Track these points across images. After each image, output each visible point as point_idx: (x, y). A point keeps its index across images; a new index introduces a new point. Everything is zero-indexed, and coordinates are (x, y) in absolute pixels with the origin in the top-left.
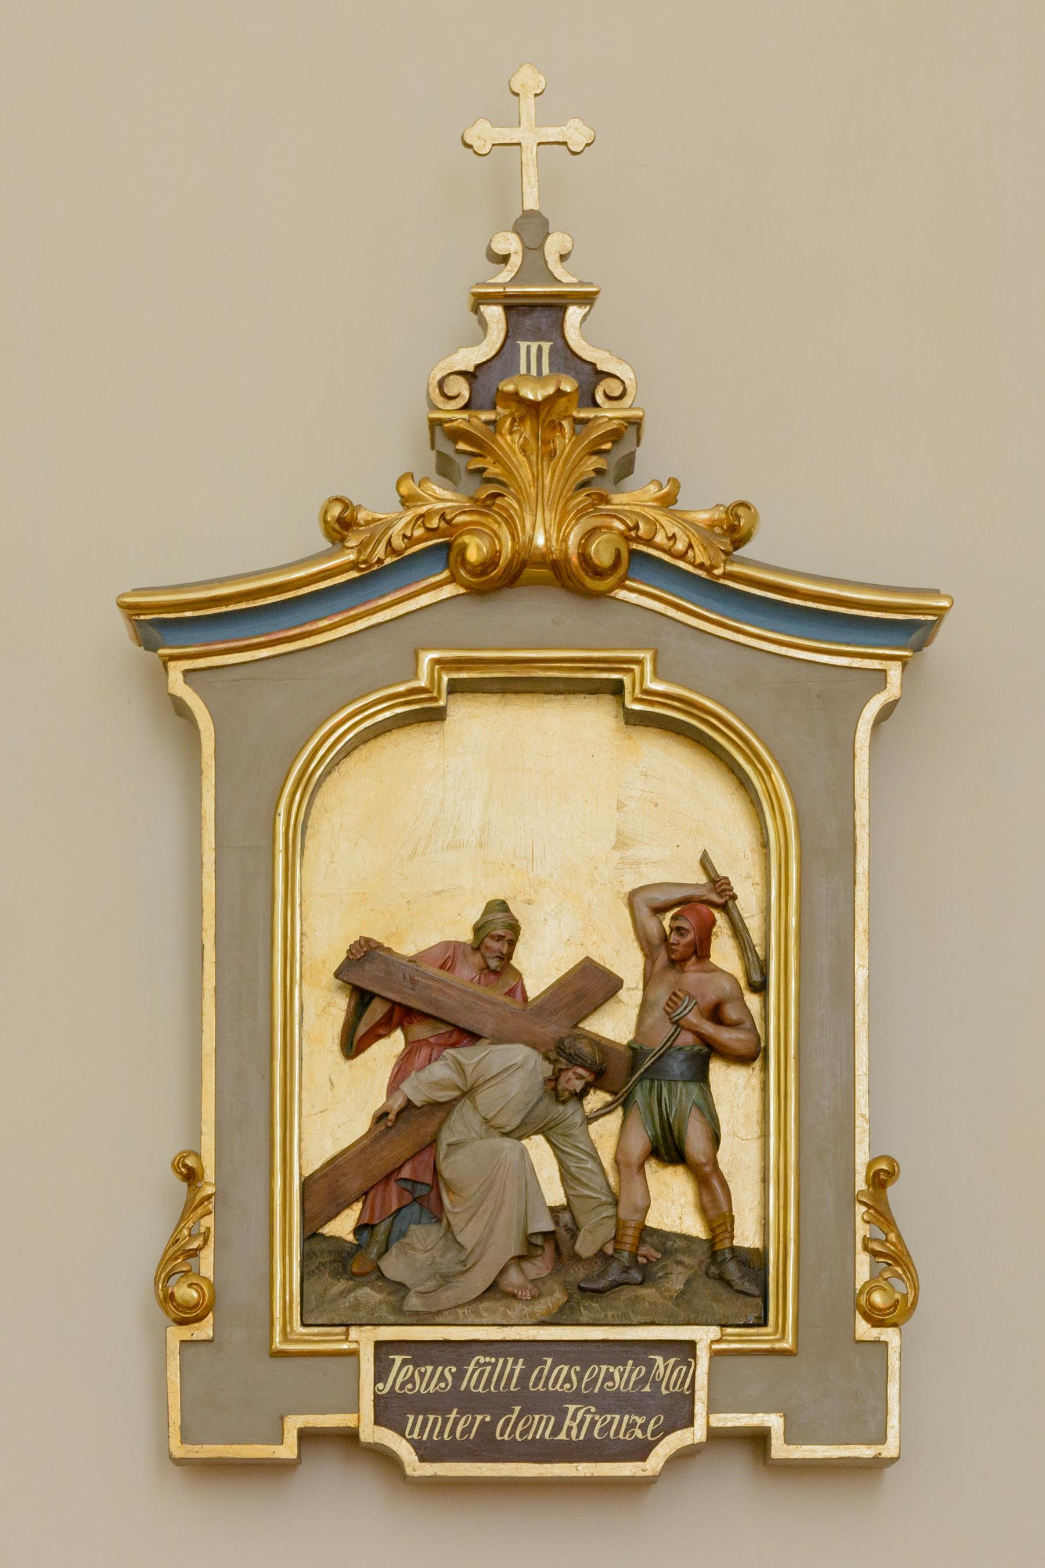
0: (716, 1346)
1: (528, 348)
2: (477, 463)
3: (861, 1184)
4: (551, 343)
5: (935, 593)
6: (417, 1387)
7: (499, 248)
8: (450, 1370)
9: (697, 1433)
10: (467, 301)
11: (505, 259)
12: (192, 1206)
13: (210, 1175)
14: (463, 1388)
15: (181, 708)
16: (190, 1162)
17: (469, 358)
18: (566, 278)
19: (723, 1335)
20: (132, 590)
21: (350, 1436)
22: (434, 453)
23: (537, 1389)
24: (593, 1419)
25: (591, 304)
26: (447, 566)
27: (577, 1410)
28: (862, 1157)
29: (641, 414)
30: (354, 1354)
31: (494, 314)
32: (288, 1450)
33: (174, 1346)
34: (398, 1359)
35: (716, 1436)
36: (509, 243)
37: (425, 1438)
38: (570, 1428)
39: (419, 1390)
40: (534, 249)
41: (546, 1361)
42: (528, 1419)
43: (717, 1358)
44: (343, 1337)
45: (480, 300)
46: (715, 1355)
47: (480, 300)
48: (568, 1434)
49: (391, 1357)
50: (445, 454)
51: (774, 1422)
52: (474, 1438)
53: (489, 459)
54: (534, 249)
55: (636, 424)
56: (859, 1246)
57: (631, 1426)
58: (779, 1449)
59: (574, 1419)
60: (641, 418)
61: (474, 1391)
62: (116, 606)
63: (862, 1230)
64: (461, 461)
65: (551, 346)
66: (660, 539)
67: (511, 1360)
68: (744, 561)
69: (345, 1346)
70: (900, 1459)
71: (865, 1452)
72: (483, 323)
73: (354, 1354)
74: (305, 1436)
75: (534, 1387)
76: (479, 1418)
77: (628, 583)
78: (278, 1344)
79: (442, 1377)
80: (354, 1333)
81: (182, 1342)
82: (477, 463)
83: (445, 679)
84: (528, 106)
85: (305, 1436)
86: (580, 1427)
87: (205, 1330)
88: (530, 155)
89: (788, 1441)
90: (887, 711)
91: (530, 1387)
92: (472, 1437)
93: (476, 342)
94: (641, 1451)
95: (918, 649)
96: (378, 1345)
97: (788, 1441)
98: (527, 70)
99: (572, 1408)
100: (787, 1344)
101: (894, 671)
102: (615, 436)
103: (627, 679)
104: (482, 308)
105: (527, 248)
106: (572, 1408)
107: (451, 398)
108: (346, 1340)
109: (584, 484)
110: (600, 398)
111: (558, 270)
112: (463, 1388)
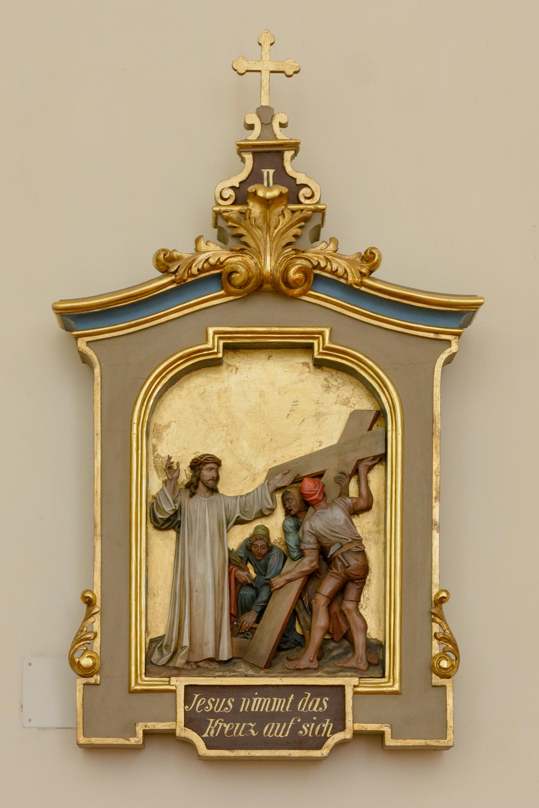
1: (268, 173)
5: (474, 297)
7: (249, 122)
9: (347, 735)
10: (235, 148)
11: (251, 127)
13: (98, 603)
14: (241, 710)
15: (85, 359)
18: (281, 136)
19: (360, 684)
20: (60, 301)
21: (170, 734)
24: (223, 726)
25: (296, 154)
26: (222, 288)
30: (174, 691)
31: (249, 158)
32: (137, 740)
35: (357, 734)
36: (253, 119)
40: (267, 124)
41: (307, 694)
44: (168, 683)
46: (355, 693)
47: (242, 149)
48: (209, 734)
49: (274, 698)
50: (221, 227)
54: (267, 124)
55: (323, 211)
56: (99, 635)
57: (247, 728)
58: (389, 742)
59: (213, 725)
60: (324, 209)
61: (217, 712)
62: (52, 309)
64: (229, 231)
68: (374, 279)
70: (454, 746)
71: (442, 743)
72: (243, 160)
73: (174, 691)
74: (147, 734)
77: (311, 292)
79: (226, 705)
80: (173, 680)
83: (221, 342)
85: (147, 734)
86: (216, 729)
87: (97, 678)
88: (266, 75)
90: (449, 360)
91: (197, 710)
95: (465, 326)
99: (212, 720)
100: (396, 687)
103: (316, 342)
105: (264, 124)
106: (212, 720)
107: (225, 200)
108: (169, 684)
109: (289, 244)
110: (302, 199)
112: (241, 710)
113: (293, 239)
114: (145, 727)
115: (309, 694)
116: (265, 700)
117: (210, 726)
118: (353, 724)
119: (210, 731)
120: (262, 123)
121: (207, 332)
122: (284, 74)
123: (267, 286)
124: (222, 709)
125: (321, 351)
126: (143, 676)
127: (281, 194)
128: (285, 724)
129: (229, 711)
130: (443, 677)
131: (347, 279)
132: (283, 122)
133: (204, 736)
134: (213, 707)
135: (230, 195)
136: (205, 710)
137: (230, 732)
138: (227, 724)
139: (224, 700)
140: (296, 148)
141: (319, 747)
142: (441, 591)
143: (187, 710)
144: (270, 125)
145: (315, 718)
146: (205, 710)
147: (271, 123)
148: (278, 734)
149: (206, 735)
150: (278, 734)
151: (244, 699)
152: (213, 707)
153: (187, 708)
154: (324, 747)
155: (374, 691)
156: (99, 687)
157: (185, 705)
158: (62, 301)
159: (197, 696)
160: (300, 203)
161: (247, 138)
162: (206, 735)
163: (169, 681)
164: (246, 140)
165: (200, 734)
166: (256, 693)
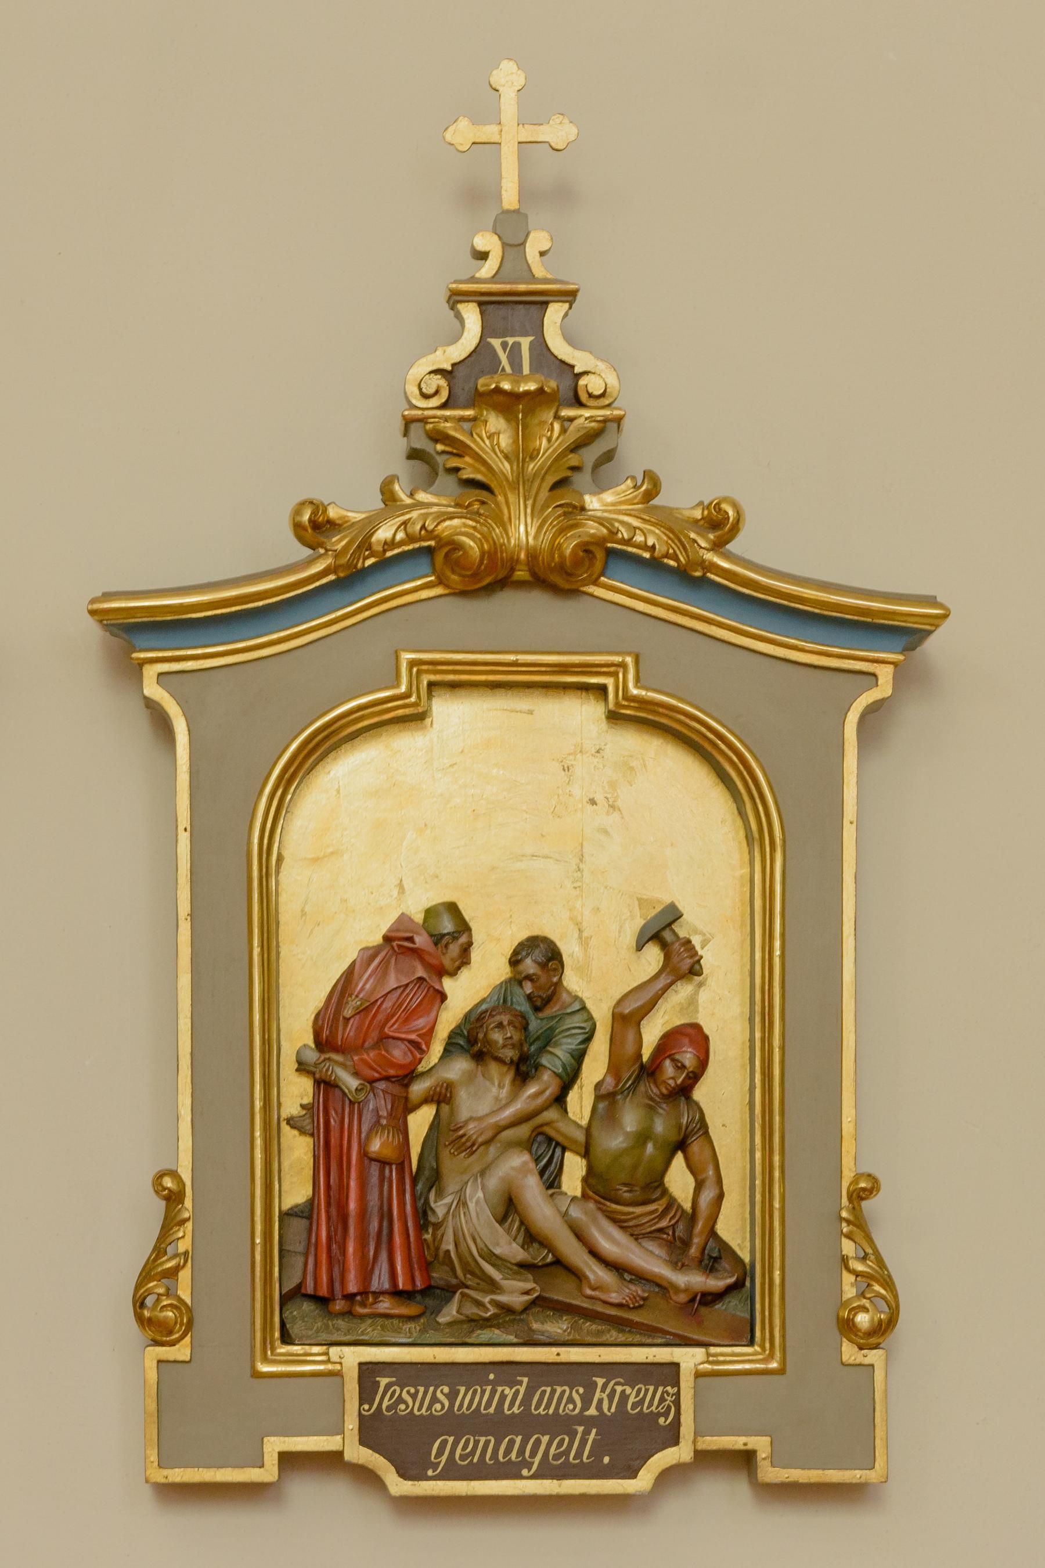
2: (454, 462)
3: (845, 1201)
4: (531, 338)
9: (680, 1453)
10: (444, 295)
11: (483, 256)
12: (170, 1223)
15: (152, 707)
16: (168, 1182)
19: (708, 1355)
21: (339, 1454)
23: (461, 1412)
28: (848, 1175)
29: (622, 413)
30: (338, 1374)
31: (471, 315)
32: (269, 1472)
33: (151, 1366)
34: (384, 1381)
35: (705, 1459)
37: (551, 1411)
38: (600, 1401)
40: (514, 247)
42: (562, 1441)
43: (701, 1380)
45: (456, 298)
47: (456, 298)
49: (378, 1379)
51: (760, 1444)
53: (467, 459)
54: (514, 247)
55: (618, 420)
58: (769, 1473)
65: (531, 342)
67: (651, 1388)
72: (459, 317)
73: (338, 1374)
75: (509, 1410)
79: (434, 1400)
82: (454, 462)
85: (287, 1460)
87: (181, 1351)
93: (455, 338)
101: (885, 674)
104: (460, 307)
105: (511, 245)
108: (329, 1361)
111: (539, 271)
114: (284, 1442)
115: (525, 1380)
116: (559, 1390)
123: (521, 574)
124: (429, 1408)
126: (278, 1343)
127: (541, 391)
129: (440, 1413)
131: (677, 559)
136: (401, 1413)
139: (432, 1389)
140: (569, 299)
143: (364, 1413)
144: (522, 247)
146: (401, 1413)
147: (523, 244)
151: (463, 1389)
154: (788, 1480)
157: (360, 1405)
158: (107, 596)
159: (384, 1381)
160: (580, 404)
161: (477, 275)
163: (327, 1354)
164: (473, 280)
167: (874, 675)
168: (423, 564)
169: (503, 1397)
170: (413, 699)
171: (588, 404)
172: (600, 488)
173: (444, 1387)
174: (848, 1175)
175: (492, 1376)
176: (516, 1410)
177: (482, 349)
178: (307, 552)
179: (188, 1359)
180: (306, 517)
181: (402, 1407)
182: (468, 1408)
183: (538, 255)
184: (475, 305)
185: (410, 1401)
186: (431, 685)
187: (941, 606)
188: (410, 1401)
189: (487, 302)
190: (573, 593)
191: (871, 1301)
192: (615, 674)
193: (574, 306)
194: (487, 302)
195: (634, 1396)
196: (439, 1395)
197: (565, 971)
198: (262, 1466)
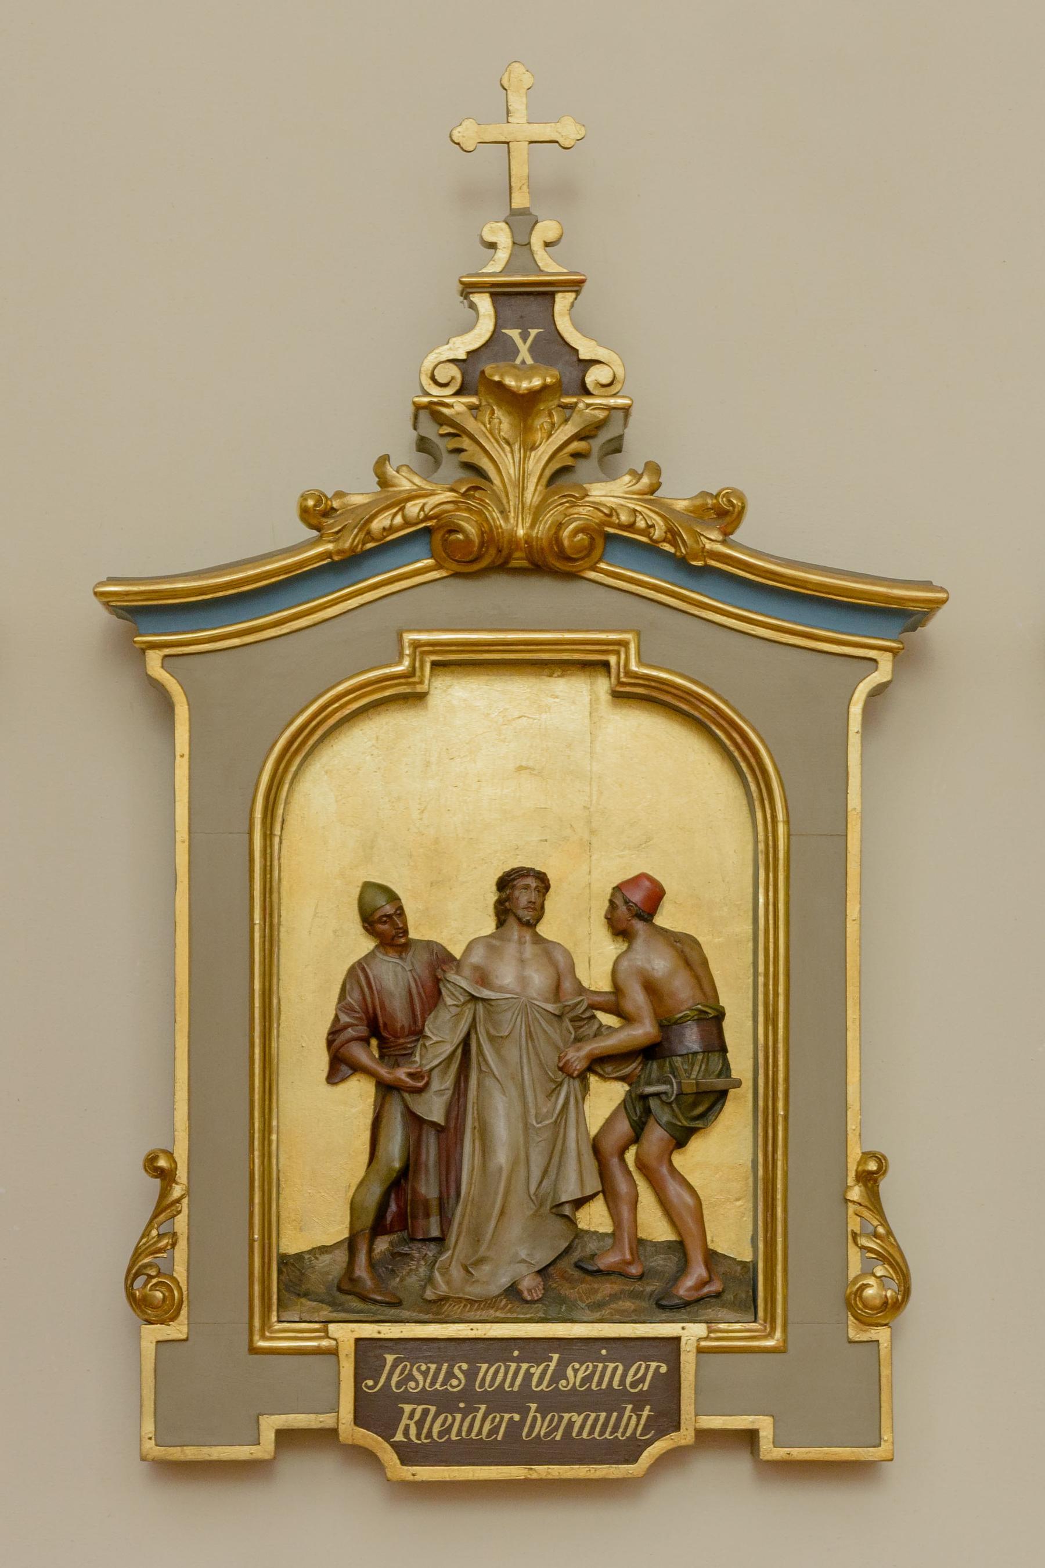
0: (703, 1344)
2: (453, 444)
4: (520, 331)
5: (927, 585)
6: (571, 1381)
8: (460, 1368)
9: (685, 1436)
13: (182, 1174)
16: (162, 1163)
17: (461, 347)
19: (710, 1331)
21: (331, 1434)
22: (415, 433)
25: (577, 292)
27: (413, 1412)
28: (855, 1153)
29: (627, 401)
30: (333, 1352)
31: (484, 303)
33: (148, 1348)
34: (390, 1358)
35: (705, 1437)
36: (502, 236)
37: (604, 1386)
39: (424, 1386)
43: (705, 1357)
45: (468, 289)
46: (700, 1351)
47: (468, 289)
51: (765, 1425)
52: (562, 1438)
54: (521, 246)
55: (626, 410)
58: (768, 1450)
59: (411, 1417)
61: (633, 1391)
63: (854, 1224)
66: (641, 524)
69: (325, 1343)
72: (473, 306)
73: (333, 1352)
75: (537, 1387)
76: (507, 1416)
77: (602, 565)
78: (409, 637)
79: (450, 1375)
81: (158, 1342)
84: (518, 103)
85: (285, 1437)
87: (177, 1330)
89: (776, 1444)
90: (878, 691)
92: (500, 1438)
94: (630, 1451)
96: (360, 1342)
97: (776, 1444)
98: (518, 69)
99: (408, 1408)
102: (600, 425)
111: (542, 257)
113: (570, 462)
117: (404, 1421)
118: (696, 1415)
119: (407, 1429)
120: (514, 243)
121: (400, 640)
122: (457, 146)
125: (623, 650)
128: (615, 1414)
130: (865, 1322)
132: (551, 236)
133: (396, 1439)
134: (425, 1382)
135: (453, 378)
137: (446, 1431)
138: (579, 1415)
139: (445, 1365)
141: (633, 1459)
142: (867, 1155)
144: (528, 246)
145: (462, 1405)
147: (529, 243)
148: (602, 1433)
149: (399, 1437)
150: (602, 1433)
152: (425, 1382)
153: (565, 1385)
155: (295, 1346)
156: (185, 1343)
158: (112, 580)
160: (587, 393)
162: (399, 1437)
163: (326, 1331)
165: (387, 1435)
166: (604, 1352)
167: (875, 661)
168: (419, 547)
169: (528, 1376)
170: (416, 679)
171: (594, 393)
172: (610, 474)
173: (664, 1365)
174: (855, 1153)
175: (516, 1353)
176: (543, 1386)
177: (496, 337)
178: (315, 533)
179: (184, 1337)
180: (311, 503)
181: (412, 1384)
182: (490, 1386)
183: (542, 243)
184: (487, 295)
185: (420, 1378)
186: (435, 664)
187: (942, 590)
188: (420, 1378)
189: (500, 293)
190: (573, 576)
191: (882, 1280)
192: (618, 653)
193: (579, 297)
194: (500, 293)
195: (582, 1372)
196: (456, 1371)
197: (614, 958)
198: (259, 1444)
